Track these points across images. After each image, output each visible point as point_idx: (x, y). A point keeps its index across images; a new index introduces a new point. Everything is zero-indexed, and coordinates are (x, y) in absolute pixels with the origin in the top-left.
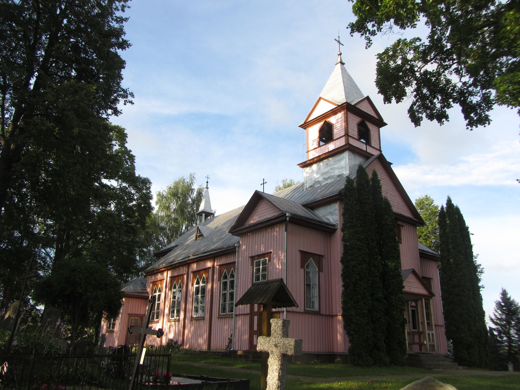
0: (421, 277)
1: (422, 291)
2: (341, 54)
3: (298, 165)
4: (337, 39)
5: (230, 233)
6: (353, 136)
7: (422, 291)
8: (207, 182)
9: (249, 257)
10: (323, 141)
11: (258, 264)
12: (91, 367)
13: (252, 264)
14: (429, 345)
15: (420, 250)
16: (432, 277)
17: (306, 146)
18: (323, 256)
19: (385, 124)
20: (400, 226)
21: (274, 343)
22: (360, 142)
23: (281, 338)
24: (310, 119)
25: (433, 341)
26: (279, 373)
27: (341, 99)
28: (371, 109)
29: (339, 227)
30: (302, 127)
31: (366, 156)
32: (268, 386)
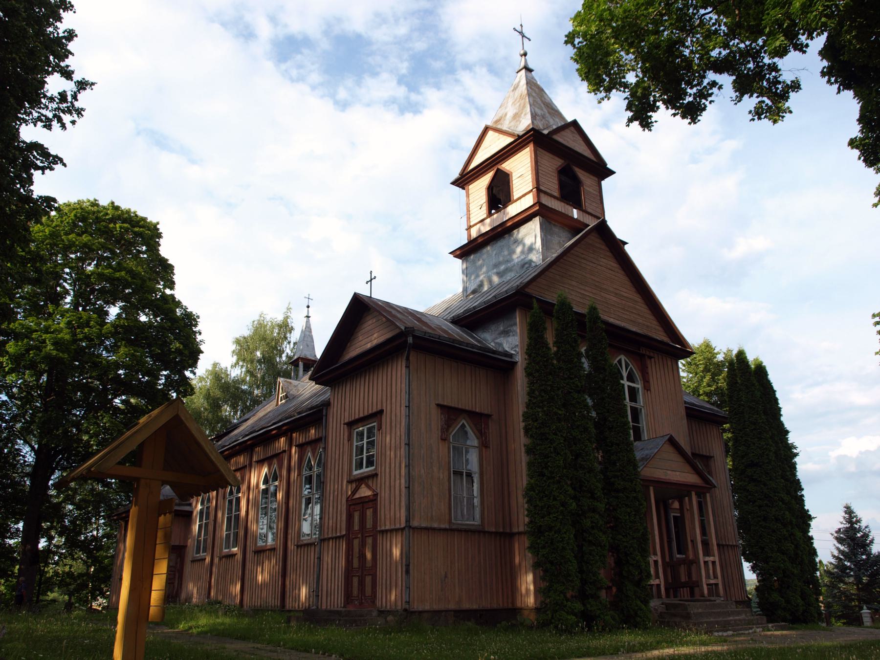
0: (690, 454)
1: (689, 477)
2: (525, 54)
4: (519, 29)
6: (548, 191)
7: (689, 477)
8: (308, 307)
11: (361, 435)
12: (335, 600)
14: (708, 585)
15: (685, 402)
16: (712, 455)
17: (465, 219)
18: (489, 416)
20: (646, 357)
24: (473, 165)
25: (715, 577)
27: (524, 124)
29: (520, 358)
30: (458, 186)
31: (575, 227)
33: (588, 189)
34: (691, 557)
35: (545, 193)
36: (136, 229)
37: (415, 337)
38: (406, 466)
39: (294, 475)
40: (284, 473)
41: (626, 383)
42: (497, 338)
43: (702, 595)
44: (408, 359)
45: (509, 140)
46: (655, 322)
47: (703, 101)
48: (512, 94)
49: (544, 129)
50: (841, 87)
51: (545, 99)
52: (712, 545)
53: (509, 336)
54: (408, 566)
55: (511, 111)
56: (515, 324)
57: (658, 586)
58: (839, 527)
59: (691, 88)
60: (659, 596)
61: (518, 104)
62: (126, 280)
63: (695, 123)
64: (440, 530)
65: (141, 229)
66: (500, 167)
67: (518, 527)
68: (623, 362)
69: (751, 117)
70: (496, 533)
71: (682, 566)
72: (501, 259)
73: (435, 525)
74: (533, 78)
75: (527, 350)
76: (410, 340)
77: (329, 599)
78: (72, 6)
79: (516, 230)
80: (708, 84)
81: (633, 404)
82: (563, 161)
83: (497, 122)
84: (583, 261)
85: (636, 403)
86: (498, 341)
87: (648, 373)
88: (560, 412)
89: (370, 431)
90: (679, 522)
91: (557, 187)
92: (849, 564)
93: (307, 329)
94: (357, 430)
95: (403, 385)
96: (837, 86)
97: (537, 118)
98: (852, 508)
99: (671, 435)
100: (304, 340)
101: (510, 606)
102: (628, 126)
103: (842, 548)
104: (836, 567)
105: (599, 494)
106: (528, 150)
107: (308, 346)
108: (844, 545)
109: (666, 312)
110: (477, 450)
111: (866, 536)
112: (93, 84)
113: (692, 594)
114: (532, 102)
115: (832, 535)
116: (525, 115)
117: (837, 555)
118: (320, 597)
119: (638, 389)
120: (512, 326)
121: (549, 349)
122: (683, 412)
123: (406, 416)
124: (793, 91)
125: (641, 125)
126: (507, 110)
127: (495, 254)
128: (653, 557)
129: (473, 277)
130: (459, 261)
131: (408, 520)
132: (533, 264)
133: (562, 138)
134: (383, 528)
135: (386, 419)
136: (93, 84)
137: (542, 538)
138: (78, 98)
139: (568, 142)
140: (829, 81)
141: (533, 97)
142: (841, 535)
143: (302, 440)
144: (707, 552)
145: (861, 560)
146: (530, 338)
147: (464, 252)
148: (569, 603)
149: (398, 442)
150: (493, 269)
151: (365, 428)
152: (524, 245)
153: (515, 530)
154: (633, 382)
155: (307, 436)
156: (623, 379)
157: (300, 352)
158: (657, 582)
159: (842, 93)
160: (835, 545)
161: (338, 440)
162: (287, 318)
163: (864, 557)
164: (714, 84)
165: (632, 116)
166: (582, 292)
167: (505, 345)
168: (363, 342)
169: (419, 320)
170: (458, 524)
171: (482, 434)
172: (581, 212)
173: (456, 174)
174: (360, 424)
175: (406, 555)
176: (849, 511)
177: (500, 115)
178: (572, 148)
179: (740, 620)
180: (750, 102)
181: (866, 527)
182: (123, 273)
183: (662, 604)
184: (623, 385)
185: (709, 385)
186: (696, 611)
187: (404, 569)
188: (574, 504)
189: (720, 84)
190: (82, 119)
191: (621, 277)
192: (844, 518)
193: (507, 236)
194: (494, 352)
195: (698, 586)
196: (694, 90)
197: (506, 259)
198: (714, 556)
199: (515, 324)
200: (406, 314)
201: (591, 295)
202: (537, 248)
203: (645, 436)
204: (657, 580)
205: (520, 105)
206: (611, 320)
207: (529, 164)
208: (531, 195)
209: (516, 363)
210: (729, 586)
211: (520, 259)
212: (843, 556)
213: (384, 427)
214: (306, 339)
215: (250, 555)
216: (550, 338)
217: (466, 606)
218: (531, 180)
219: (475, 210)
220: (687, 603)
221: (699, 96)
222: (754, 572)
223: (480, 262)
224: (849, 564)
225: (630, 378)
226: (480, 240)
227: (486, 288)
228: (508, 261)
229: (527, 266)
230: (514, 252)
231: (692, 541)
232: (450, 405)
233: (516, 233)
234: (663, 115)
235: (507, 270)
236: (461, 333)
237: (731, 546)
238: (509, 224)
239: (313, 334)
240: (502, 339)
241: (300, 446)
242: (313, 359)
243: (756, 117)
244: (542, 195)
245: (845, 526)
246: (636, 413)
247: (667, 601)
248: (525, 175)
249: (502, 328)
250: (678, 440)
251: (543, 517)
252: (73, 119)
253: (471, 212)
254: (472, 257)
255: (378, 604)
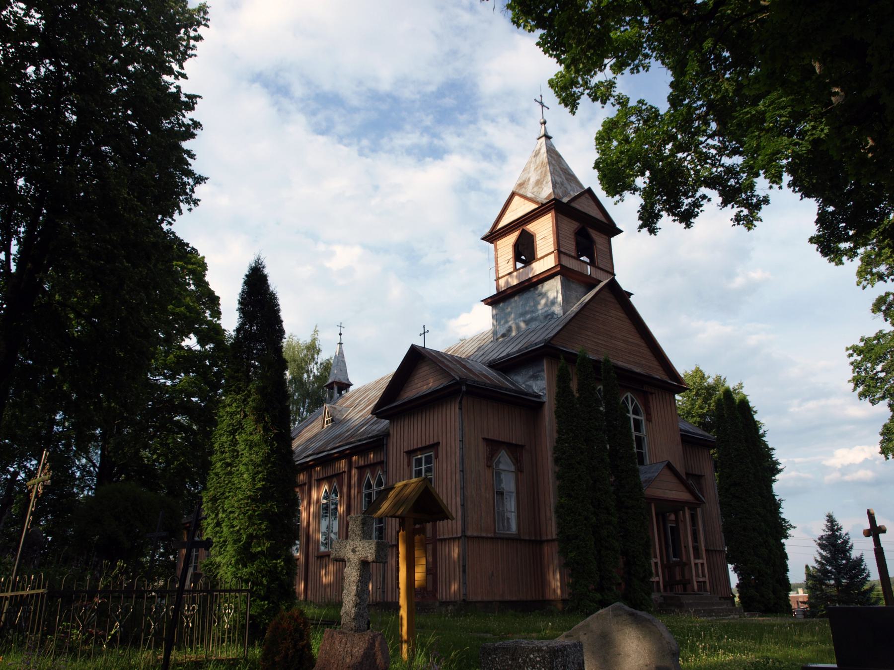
1: (682, 495)
2: (545, 123)
3: (482, 301)
4: (539, 99)
5: (373, 414)
6: (568, 252)
7: (682, 495)
8: (340, 334)
9: (404, 452)
10: (521, 261)
13: (409, 464)
14: (697, 582)
15: (681, 430)
16: (703, 474)
17: (494, 270)
18: (522, 447)
19: (620, 231)
21: (351, 548)
22: (579, 262)
23: (360, 540)
24: (501, 225)
25: (704, 576)
26: (358, 586)
27: (546, 192)
28: (596, 207)
30: (487, 241)
31: (590, 283)
32: (344, 604)
33: (600, 247)
34: (684, 560)
35: (565, 254)
36: (190, 267)
37: (467, 385)
38: (461, 489)
39: (354, 492)
40: (345, 490)
41: (632, 416)
42: (527, 381)
43: (693, 591)
44: (460, 403)
45: (534, 206)
46: (656, 363)
47: (696, 210)
48: (534, 160)
49: (564, 196)
50: (803, 196)
51: (562, 165)
52: (702, 550)
53: (537, 380)
54: (464, 566)
55: (534, 178)
56: (543, 371)
57: (658, 582)
58: (822, 535)
59: (687, 198)
60: (659, 590)
61: (540, 171)
62: (185, 315)
63: (689, 228)
64: (487, 538)
65: (194, 266)
66: (525, 228)
67: (547, 535)
68: (629, 398)
69: (732, 223)
70: (530, 541)
71: (677, 567)
72: (527, 309)
73: (484, 535)
74: (552, 145)
75: (556, 396)
76: (464, 388)
77: (394, 594)
78: (201, 125)
79: (540, 285)
80: (700, 197)
81: (638, 434)
82: (579, 224)
83: (521, 185)
84: (598, 314)
85: (640, 432)
86: (528, 383)
87: (649, 407)
88: (583, 447)
89: (429, 460)
90: (675, 531)
91: (574, 247)
92: (830, 568)
93: (340, 355)
94: (416, 457)
95: (457, 424)
96: (800, 194)
97: (557, 186)
98: (834, 517)
99: (669, 462)
100: (337, 365)
101: (541, 598)
102: (639, 231)
103: (824, 553)
104: (819, 571)
105: (613, 511)
106: (549, 215)
107: (341, 370)
108: (826, 551)
109: (666, 355)
110: (514, 475)
111: (846, 542)
112: (207, 179)
113: (685, 589)
114: (552, 170)
115: (816, 541)
116: (547, 183)
117: (819, 560)
118: (386, 593)
119: (642, 420)
120: (539, 372)
121: (573, 396)
122: (679, 439)
123: (460, 448)
124: (764, 204)
125: (649, 230)
126: (530, 175)
127: (522, 305)
128: (654, 559)
129: (502, 322)
130: (490, 308)
131: (463, 531)
132: (555, 316)
133: (579, 205)
134: (442, 537)
135: (442, 450)
136: (207, 179)
137: (570, 544)
138: (195, 190)
139: (583, 207)
140: (794, 191)
141: (553, 165)
142: (824, 542)
143: (362, 463)
144: (697, 555)
145: (841, 565)
146: (559, 388)
147: (492, 301)
148: (591, 594)
149: (453, 469)
150: (520, 317)
151: (423, 456)
152: (548, 298)
153: (544, 538)
154: (637, 415)
155: (366, 459)
156: (629, 413)
157: (334, 376)
158: (657, 579)
159: (804, 199)
160: (818, 551)
161: (398, 464)
162: (314, 341)
163: (844, 562)
164: (704, 197)
165: (642, 224)
166: (596, 340)
167: (534, 387)
168: (419, 385)
169: (464, 367)
170: (501, 534)
171: (517, 462)
172: (594, 268)
173: (486, 231)
174: (419, 453)
175: (463, 556)
176: (831, 519)
177: (524, 179)
178: (588, 213)
179: (722, 609)
180: (731, 211)
181: (846, 534)
182: (183, 309)
183: (661, 596)
184: (630, 418)
185: (701, 408)
186: (687, 602)
187: (461, 569)
188: (594, 518)
189: (709, 197)
190: (197, 208)
191: (627, 325)
192: (827, 525)
193: (532, 289)
194: (526, 394)
195: (689, 583)
196: (690, 200)
197: (531, 310)
198: (703, 559)
199: (543, 371)
200: (454, 363)
201: (603, 343)
202: (559, 302)
203: (647, 461)
204: (657, 578)
205: (541, 172)
206: (620, 364)
207: (551, 229)
208: (552, 256)
209: (543, 403)
210: (716, 586)
211: (543, 311)
212: (826, 561)
213: (440, 456)
214: (339, 364)
215: (312, 560)
216: (574, 385)
217: (508, 598)
218: (552, 242)
219: (503, 263)
220: (680, 596)
221: (693, 206)
222: (736, 572)
223: (509, 309)
224: (830, 568)
225: (636, 412)
226: (509, 292)
227: (514, 334)
228: (533, 312)
229: (549, 317)
230: (539, 303)
231: (685, 547)
232: (493, 438)
233: (540, 288)
234: (666, 221)
235: (533, 319)
236: (498, 376)
237: (718, 551)
238: (535, 280)
239: (346, 359)
240: (531, 382)
241: (361, 469)
242: (346, 382)
243: (736, 223)
244: (562, 256)
245: (827, 533)
246: (640, 441)
247: (665, 594)
248: (547, 238)
249: (531, 373)
250: (675, 466)
251: (571, 529)
252: (190, 207)
253: (499, 265)
254: (501, 305)
255: (439, 596)
